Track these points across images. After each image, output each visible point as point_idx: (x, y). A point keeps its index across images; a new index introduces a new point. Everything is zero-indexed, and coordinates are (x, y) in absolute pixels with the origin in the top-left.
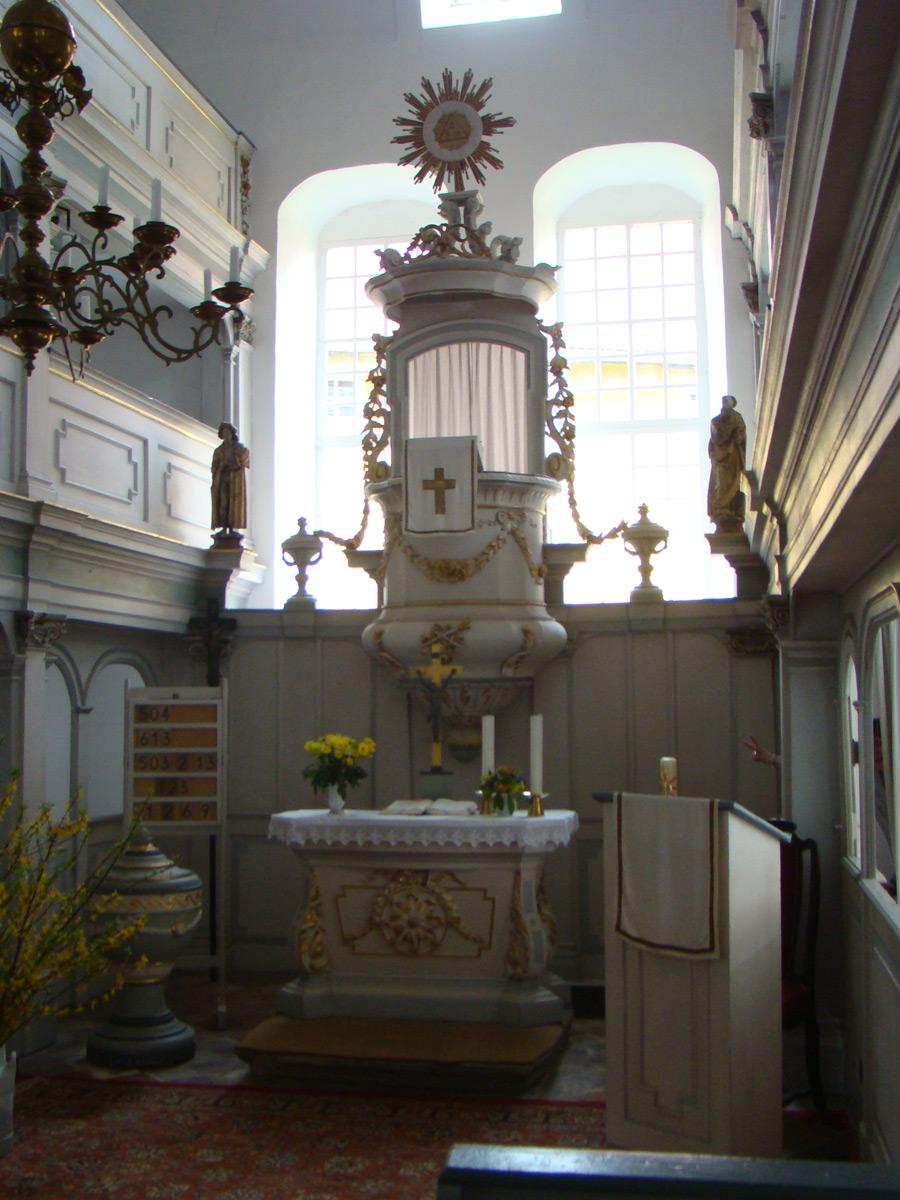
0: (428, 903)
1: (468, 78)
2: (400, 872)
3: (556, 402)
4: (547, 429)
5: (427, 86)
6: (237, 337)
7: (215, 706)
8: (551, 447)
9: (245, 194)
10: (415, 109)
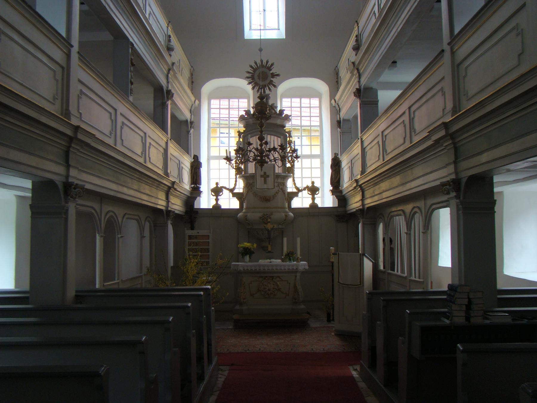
0: (273, 284)
1: (267, 62)
2: (266, 277)
3: (289, 152)
4: (287, 160)
5: (256, 63)
6: (191, 128)
7: (209, 235)
8: (288, 165)
9: (192, 85)
10: (252, 69)
